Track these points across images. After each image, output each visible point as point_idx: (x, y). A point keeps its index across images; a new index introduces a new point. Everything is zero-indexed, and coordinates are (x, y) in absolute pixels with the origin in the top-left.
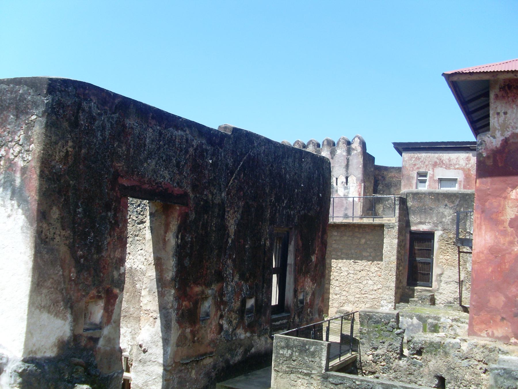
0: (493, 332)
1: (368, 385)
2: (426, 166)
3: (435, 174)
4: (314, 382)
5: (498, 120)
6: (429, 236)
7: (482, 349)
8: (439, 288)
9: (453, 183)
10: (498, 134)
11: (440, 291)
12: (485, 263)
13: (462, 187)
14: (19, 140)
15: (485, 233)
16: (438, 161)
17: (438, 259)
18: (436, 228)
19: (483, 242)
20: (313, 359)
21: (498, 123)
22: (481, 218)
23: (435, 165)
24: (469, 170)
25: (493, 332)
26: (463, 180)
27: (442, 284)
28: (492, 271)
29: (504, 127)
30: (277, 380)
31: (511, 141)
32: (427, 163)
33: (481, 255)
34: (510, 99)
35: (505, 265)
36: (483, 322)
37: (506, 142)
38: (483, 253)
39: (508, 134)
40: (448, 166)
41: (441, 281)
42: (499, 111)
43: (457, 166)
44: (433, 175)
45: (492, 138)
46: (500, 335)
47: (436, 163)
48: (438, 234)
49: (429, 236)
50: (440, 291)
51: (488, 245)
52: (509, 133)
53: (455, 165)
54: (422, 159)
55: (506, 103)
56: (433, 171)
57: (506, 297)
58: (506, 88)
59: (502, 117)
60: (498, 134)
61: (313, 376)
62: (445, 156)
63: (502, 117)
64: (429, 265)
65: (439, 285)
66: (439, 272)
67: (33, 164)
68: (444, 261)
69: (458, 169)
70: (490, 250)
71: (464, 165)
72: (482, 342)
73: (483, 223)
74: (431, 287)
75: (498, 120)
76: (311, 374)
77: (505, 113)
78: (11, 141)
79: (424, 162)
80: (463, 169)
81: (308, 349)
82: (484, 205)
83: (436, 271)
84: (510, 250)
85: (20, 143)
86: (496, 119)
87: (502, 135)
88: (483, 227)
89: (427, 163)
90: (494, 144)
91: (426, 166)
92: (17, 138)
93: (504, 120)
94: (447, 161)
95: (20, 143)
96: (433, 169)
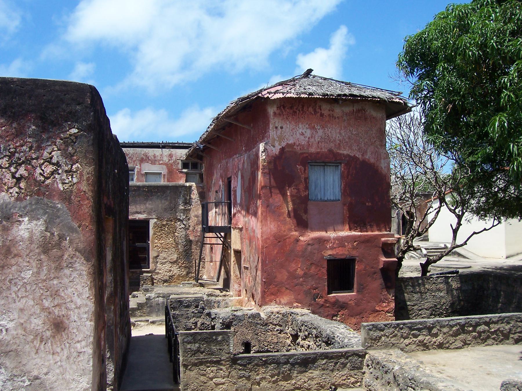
0: (280, 300)
1: (274, 359)
2: (134, 161)
3: (142, 169)
4: (224, 368)
5: (277, 133)
6: (145, 223)
7: (277, 315)
8: (156, 269)
9: (158, 176)
10: (277, 144)
11: (157, 271)
12: (271, 247)
13: (166, 180)
14: (51, 158)
15: (270, 223)
16: (144, 157)
17: (153, 242)
18: (150, 217)
19: (269, 230)
20: (220, 347)
21: (277, 135)
22: (266, 211)
23: (142, 161)
24: (172, 165)
25: (280, 300)
26: (166, 173)
27: (159, 265)
28: (277, 253)
29: (281, 138)
30: (186, 373)
31: (287, 149)
32: (134, 159)
33: (268, 241)
34: (285, 117)
35: (286, 247)
36: (272, 294)
37: (282, 150)
38: (269, 239)
39: (284, 144)
40: (154, 161)
41: (157, 262)
42: (277, 126)
43: (161, 162)
44: (140, 169)
45: (272, 147)
46: (286, 302)
47: (142, 158)
48: (152, 222)
49: (145, 223)
50: (157, 271)
51: (272, 233)
52: (285, 144)
53: (160, 160)
54: (130, 155)
55: (282, 120)
56: (140, 166)
57: (289, 272)
58: (282, 108)
59: (280, 130)
60: (277, 144)
61: (222, 362)
62: (151, 152)
63: (280, 130)
64: (146, 250)
65: (156, 265)
66: (155, 255)
67: (84, 187)
68: (159, 245)
69: (162, 164)
70: (274, 237)
71: (167, 161)
72: (276, 310)
73: (268, 215)
74: (149, 268)
75: (277, 133)
76: (221, 360)
77: (282, 128)
78: (37, 159)
79: (132, 158)
80: (166, 164)
81: (216, 339)
82: (268, 201)
83: (152, 254)
84: (289, 236)
85: (54, 160)
86: (275, 132)
87: (279, 145)
88: (269, 219)
89: (134, 159)
90: (274, 151)
91: (134, 161)
92: (46, 154)
93: (281, 133)
94: (153, 157)
95: (54, 160)
96: (140, 164)
